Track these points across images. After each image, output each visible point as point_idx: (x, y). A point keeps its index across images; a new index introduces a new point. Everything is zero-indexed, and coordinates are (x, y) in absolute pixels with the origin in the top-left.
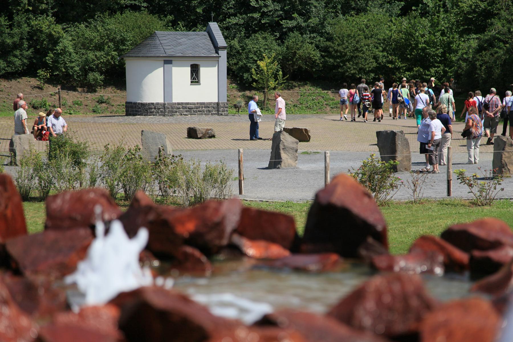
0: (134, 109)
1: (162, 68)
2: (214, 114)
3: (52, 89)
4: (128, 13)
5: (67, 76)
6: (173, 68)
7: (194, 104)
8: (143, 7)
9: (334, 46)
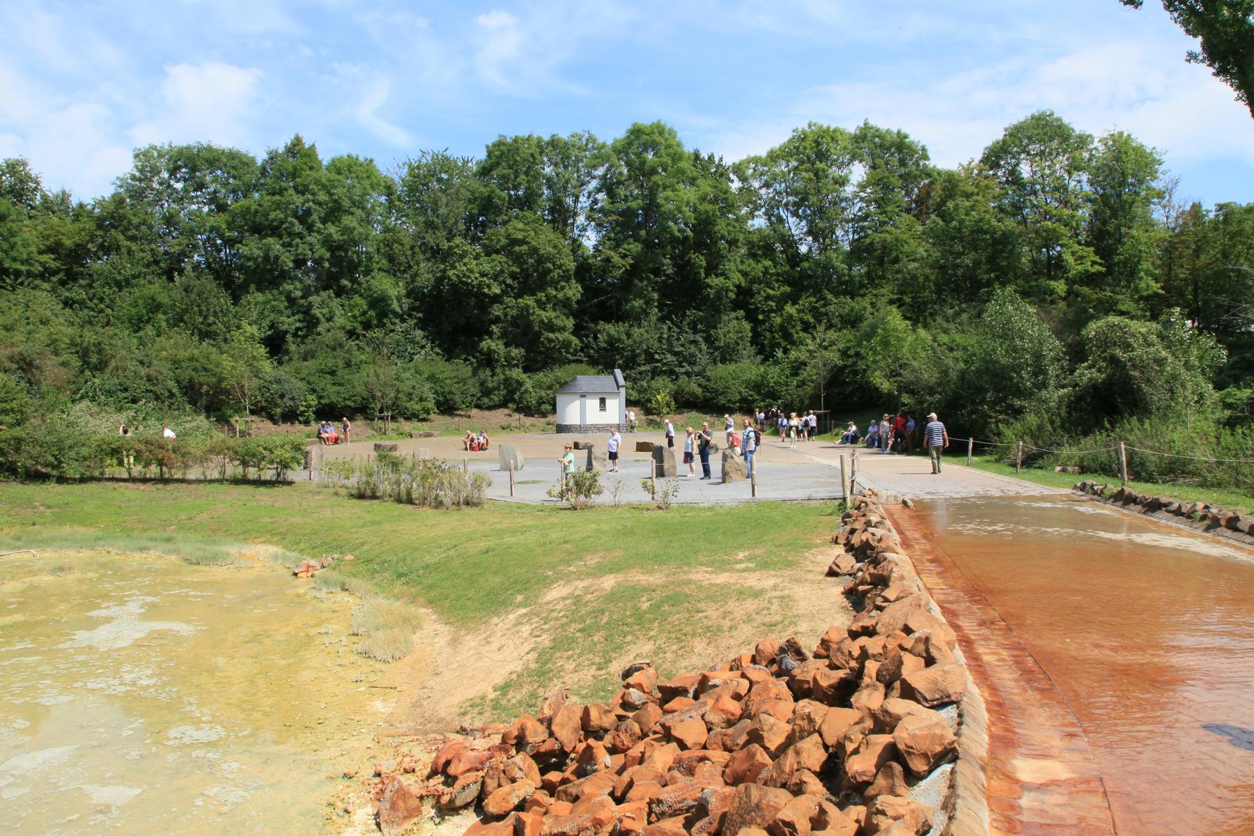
0: (561, 429)
3: (517, 416)
4: (573, 365)
5: (528, 408)
9: (711, 385)
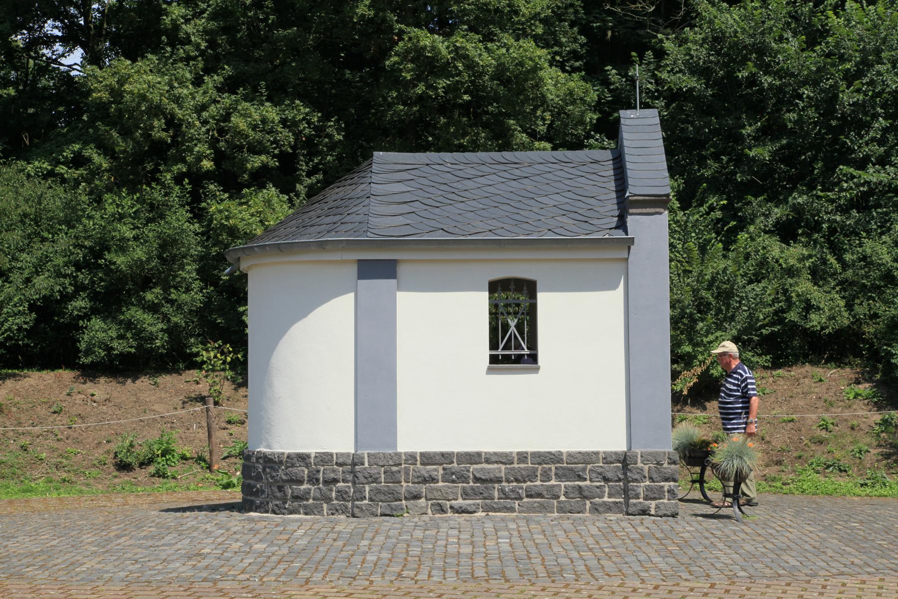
2: (609, 508)
7: (503, 459)
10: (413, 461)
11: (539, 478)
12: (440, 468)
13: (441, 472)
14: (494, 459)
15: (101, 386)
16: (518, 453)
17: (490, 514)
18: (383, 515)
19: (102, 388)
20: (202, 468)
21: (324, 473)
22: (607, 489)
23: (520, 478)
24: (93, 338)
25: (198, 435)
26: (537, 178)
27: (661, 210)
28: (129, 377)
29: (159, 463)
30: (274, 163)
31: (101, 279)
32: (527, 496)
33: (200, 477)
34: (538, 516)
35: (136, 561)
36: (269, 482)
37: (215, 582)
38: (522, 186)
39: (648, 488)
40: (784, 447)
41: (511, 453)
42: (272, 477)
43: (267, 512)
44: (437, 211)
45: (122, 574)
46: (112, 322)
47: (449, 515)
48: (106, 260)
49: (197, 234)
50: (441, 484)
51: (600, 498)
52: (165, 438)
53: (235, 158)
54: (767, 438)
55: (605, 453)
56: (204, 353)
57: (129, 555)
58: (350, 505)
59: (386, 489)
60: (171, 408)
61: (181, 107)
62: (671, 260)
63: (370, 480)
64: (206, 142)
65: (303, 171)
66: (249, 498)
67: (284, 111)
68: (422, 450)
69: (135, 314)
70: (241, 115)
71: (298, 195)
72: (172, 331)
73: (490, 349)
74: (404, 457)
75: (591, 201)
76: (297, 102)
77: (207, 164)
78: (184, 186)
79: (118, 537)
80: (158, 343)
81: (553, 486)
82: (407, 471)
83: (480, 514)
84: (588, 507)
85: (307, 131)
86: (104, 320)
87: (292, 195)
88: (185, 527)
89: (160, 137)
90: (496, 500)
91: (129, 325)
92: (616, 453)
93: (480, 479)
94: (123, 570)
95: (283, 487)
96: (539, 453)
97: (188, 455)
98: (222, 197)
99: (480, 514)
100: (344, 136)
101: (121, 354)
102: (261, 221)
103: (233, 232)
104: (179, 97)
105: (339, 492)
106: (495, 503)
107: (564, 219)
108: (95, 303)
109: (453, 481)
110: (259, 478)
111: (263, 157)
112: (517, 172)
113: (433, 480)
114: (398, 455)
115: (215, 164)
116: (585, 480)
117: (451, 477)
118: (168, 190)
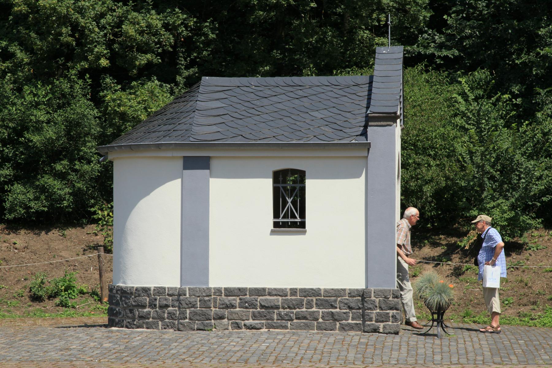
1: (180, 180)
2: (352, 327)
6: (211, 180)
7: (281, 293)
8: (325, 46)
10: (220, 294)
11: (305, 306)
12: (238, 299)
13: (238, 301)
14: (274, 293)
15: (21, 237)
16: (291, 289)
17: (271, 330)
18: (198, 330)
19: (22, 238)
20: (95, 300)
21: (159, 301)
22: (351, 315)
23: (291, 306)
24: (15, 199)
25: (94, 276)
26: (313, 97)
27: (392, 123)
28: (43, 230)
29: (63, 296)
30: (157, 60)
31: (22, 153)
32: (296, 318)
33: (92, 307)
34: (303, 332)
35: (28, 352)
36: (124, 307)
37: (72, 361)
38: (302, 104)
39: (378, 314)
40: (541, 291)
41: (286, 289)
42: (126, 303)
43: (122, 327)
44: (240, 122)
45: (18, 357)
46: (30, 186)
47: (243, 330)
48: (25, 138)
49: (95, 118)
50: (238, 309)
51: (346, 320)
52: (68, 277)
53: (126, 56)
54: (530, 285)
55: (350, 290)
56: (100, 212)
57: (25, 349)
58: (176, 322)
59: (200, 312)
60: (75, 254)
61: (83, 17)
62: (112, 225)
63: (190, 306)
64: (104, 44)
65: (182, 65)
66: (112, 317)
67: (166, 17)
68: (226, 286)
69: (48, 180)
70: (131, 22)
71: (177, 84)
72: (77, 194)
73: (274, 218)
74: (213, 291)
75: (348, 115)
76: (177, 10)
77: (104, 62)
78: (85, 80)
79: (21, 340)
80: (65, 203)
81: (314, 312)
82: (215, 302)
83: (264, 330)
84: (337, 327)
85: (185, 33)
86: (24, 185)
87: (172, 85)
88: (65, 335)
89: (67, 41)
90: (275, 321)
91: (43, 189)
92: (357, 290)
93: (265, 306)
94: (19, 355)
95: (133, 310)
96: (305, 289)
97: (85, 290)
98: (116, 88)
99: (264, 330)
100: (217, 35)
101: (37, 212)
102: (145, 108)
103: (123, 116)
104: (82, 8)
105: (169, 313)
106: (275, 323)
107: (326, 129)
108: (17, 172)
109: (246, 308)
110: (117, 304)
111: (149, 56)
112: (300, 93)
113: (233, 306)
114: (209, 289)
115: (110, 62)
116: (336, 308)
117: (247, 305)
118: (72, 83)
